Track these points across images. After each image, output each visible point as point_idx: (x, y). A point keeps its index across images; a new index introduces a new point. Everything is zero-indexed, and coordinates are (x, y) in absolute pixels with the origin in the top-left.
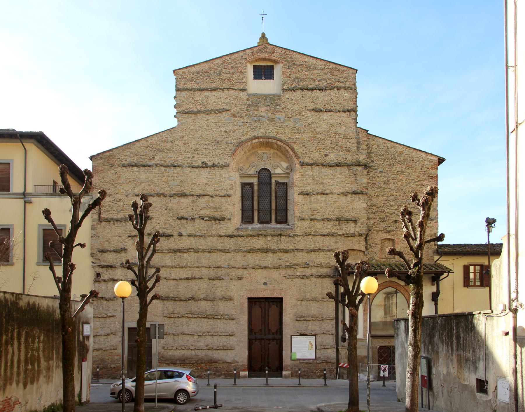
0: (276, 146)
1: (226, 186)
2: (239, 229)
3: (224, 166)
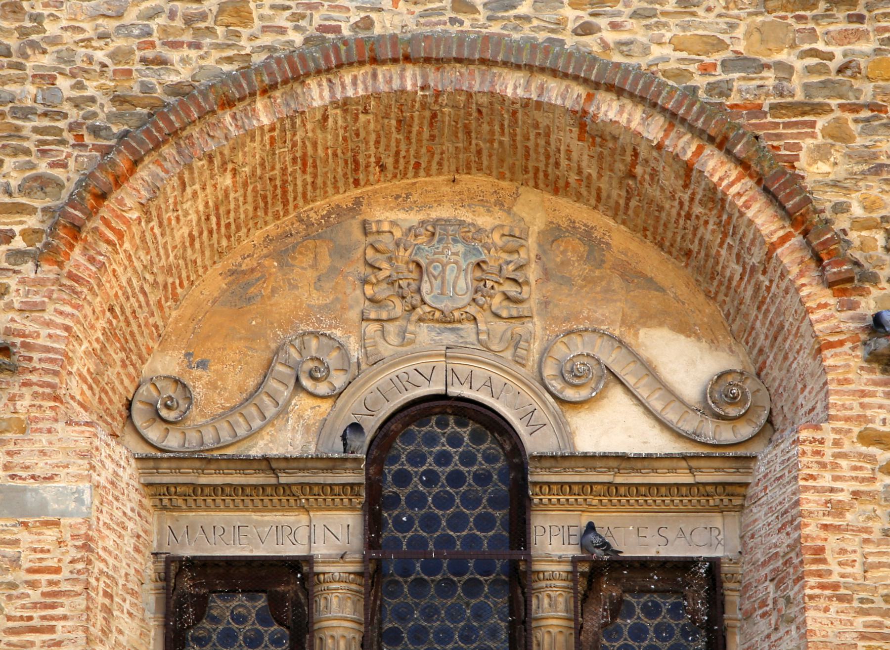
0: (580, 150)
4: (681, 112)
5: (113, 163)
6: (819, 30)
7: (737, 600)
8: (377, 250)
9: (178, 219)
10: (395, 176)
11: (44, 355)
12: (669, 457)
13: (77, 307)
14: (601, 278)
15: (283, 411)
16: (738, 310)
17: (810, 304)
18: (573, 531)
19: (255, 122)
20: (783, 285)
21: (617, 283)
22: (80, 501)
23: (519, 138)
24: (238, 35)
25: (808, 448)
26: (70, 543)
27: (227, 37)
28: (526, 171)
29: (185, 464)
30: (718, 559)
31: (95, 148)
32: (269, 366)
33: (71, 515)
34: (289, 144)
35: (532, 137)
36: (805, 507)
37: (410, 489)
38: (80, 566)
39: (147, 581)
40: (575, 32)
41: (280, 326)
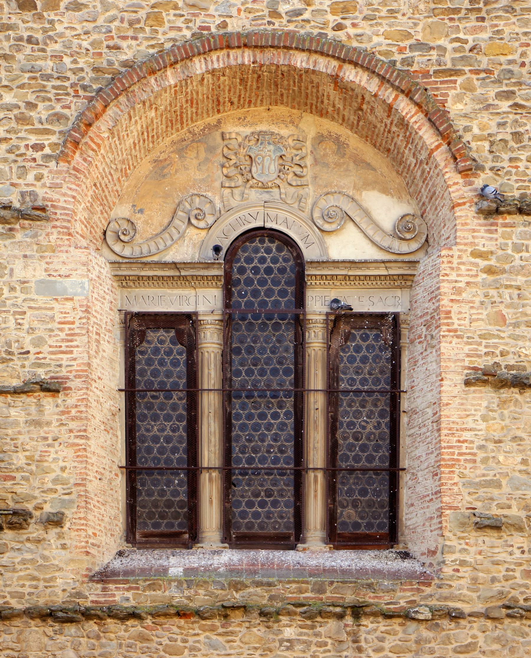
1: (32, 330)
2: (115, 573)
3: (22, 215)
4: (388, 76)
5: (94, 107)
6: (461, 26)
7: (407, 333)
8: (229, 149)
9: (128, 135)
10: (238, 107)
11: (62, 212)
12: (376, 262)
13: (78, 185)
14: (344, 163)
15: (182, 236)
16: (413, 182)
17: (450, 183)
18: (327, 298)
19: (167, 83)
20: (436, 171)
21: (352, 166)
22: (83, 288)
23: (303, 88)
24: (156, 32)
25: (445, 260)
26: (79, 309)
27: (151, 33)
28: (306, 104)
29: (134, 265)
30: (398, 313)
31: (85, 97)
32: (175, 212)
33: (79, 295)
34: (184, 93)
35: (310, 88)
36: (442, 290)
37: (245, 276)
38: (84, 321)
39: (116, 324)
40: (333, 29)
41: (180, 190)
